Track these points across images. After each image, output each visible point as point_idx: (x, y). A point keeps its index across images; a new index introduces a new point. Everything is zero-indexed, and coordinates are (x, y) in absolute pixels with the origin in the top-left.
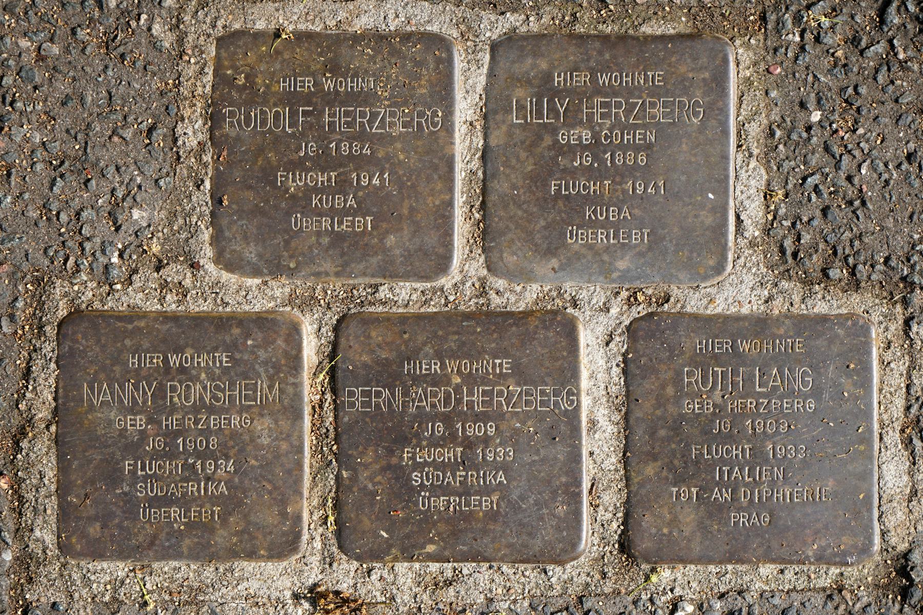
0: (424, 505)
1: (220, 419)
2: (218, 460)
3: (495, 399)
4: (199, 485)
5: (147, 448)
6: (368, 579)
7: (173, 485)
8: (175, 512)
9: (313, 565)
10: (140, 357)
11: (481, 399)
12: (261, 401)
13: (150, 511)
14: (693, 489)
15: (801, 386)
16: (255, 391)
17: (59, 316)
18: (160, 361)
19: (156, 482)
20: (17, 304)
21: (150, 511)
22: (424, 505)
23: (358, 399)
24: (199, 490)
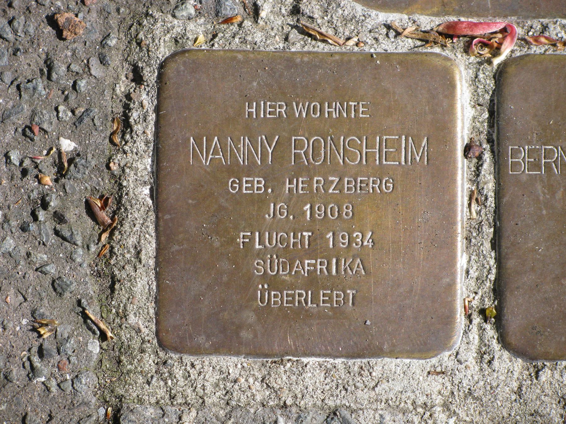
0: (262, 301)
1: (356, 182)
2: (353, 232)
3: (543, 161)
4: (329, 263)
5: (267, 216)
6: (535, 381)
7: (298, 262)
8: (300, 295)
9: (468, 363)
10: (258, 106)
11: (543, 161)
12: (406, 161)
13: (269, 294)
14: (348, 291)
15: (556, 151)
16: (399, 150)
17: (160, 56)
18: (283, 110)
19: (277, 257)
20: (109, 42)
21: (269, 294)
22: (262, 301)
23: (524, 159)
24: (329, 269)
